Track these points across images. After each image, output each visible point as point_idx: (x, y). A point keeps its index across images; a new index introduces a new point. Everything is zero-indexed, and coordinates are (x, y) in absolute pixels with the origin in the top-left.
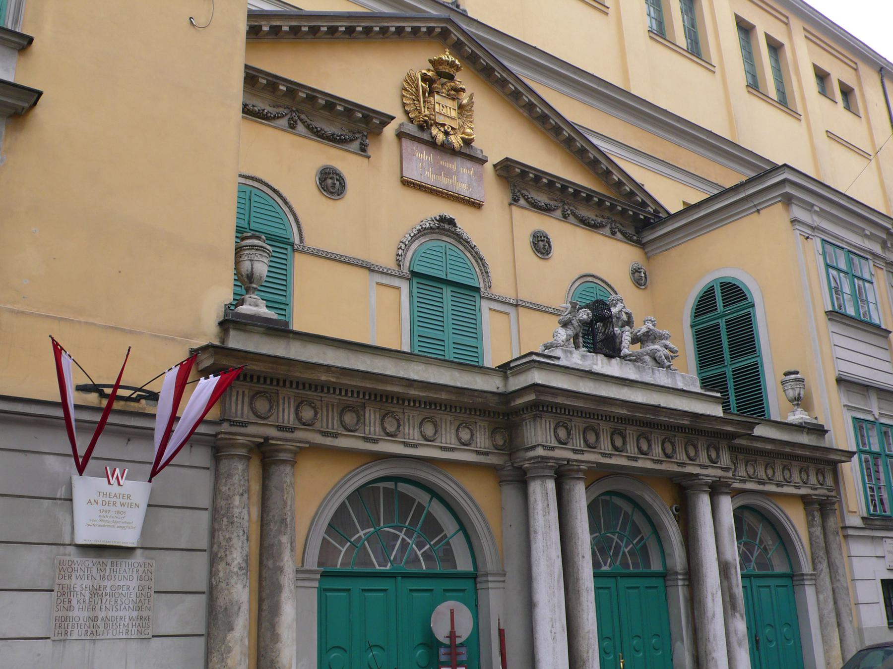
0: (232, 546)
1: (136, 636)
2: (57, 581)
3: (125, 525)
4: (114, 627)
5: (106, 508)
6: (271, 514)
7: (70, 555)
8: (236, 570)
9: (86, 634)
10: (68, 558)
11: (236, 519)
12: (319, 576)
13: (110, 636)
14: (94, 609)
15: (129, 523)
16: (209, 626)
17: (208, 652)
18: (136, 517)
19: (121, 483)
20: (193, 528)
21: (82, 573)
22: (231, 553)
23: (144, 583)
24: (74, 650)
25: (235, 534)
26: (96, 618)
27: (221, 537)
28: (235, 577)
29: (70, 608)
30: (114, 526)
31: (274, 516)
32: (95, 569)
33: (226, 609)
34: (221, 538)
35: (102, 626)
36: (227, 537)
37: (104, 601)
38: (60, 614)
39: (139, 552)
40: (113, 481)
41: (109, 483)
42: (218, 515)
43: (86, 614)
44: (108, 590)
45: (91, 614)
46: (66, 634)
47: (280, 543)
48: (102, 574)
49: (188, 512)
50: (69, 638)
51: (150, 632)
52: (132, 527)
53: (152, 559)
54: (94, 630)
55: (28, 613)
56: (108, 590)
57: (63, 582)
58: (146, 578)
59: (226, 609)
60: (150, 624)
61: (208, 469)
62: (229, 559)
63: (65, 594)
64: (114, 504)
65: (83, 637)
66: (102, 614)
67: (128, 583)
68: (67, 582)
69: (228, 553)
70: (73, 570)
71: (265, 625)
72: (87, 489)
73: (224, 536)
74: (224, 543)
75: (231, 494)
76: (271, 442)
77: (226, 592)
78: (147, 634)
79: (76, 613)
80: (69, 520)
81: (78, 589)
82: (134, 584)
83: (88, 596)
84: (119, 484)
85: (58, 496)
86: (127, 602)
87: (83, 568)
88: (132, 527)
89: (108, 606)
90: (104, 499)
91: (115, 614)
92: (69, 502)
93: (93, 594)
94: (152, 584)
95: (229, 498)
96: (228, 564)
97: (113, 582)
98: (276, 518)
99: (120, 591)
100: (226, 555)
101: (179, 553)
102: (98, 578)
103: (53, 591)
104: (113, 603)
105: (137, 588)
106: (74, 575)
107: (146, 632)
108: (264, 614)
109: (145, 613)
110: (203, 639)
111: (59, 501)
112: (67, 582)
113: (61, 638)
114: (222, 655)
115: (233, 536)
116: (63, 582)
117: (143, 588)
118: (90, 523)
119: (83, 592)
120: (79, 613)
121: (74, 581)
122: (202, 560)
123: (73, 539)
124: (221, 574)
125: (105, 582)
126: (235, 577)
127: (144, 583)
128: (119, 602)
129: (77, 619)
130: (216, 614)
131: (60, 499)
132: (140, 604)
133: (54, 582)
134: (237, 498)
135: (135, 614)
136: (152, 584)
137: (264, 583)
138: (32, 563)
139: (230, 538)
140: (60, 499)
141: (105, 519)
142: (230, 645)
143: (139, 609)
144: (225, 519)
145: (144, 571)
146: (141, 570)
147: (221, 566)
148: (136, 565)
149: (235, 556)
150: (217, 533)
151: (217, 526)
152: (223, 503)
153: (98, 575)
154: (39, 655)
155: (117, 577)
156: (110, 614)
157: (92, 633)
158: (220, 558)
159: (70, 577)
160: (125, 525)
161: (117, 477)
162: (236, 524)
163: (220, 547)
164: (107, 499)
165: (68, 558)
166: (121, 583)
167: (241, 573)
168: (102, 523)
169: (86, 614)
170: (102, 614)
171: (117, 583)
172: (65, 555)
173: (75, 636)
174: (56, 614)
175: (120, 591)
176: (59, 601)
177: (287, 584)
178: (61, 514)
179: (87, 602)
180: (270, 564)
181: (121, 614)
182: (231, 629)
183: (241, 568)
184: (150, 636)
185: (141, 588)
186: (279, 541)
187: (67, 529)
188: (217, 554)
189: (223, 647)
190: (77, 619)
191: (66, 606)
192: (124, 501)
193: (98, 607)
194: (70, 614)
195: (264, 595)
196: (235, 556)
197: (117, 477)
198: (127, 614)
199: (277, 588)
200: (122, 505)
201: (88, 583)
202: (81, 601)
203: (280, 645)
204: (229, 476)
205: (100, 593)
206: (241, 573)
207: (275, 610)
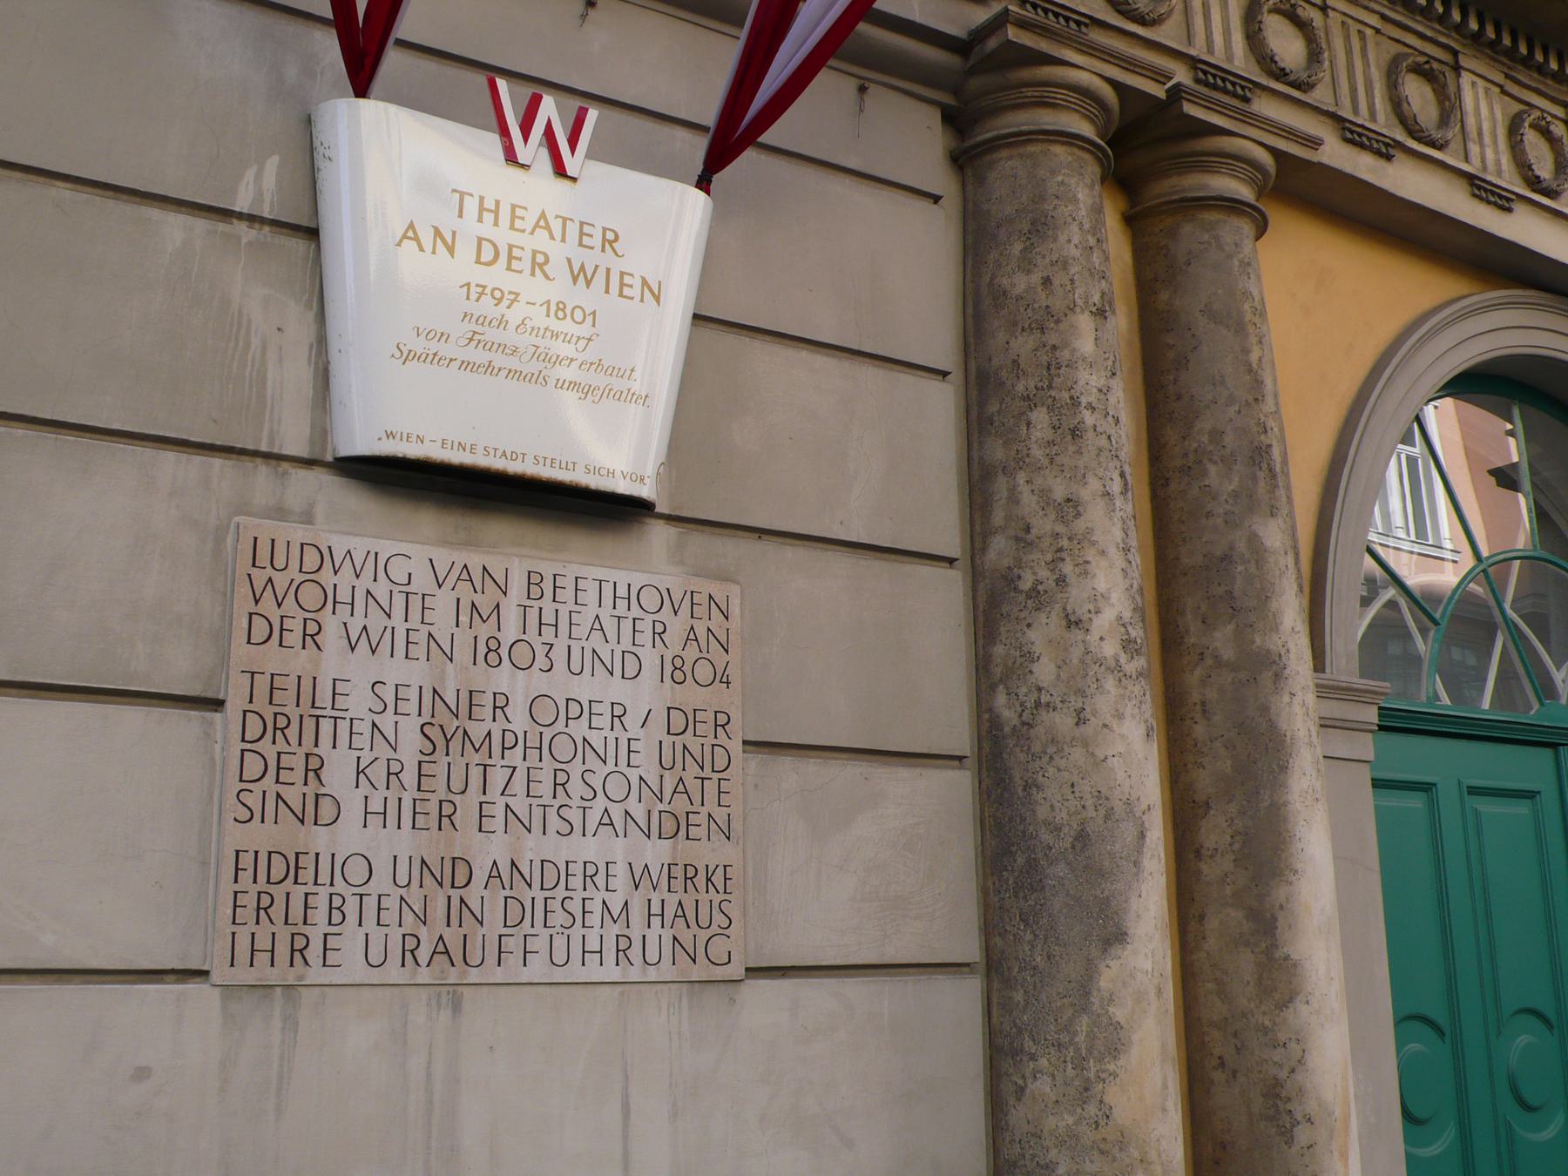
0: (1085, 539)
1: (666, 971)
2: (241, 652)
3: (600, 380)
4: (559, 918)
5: (497, 276)
6: (1204, 425)
7: (308, 518)
8: (1110, 649)
9: (409, 954)
10: (299, 534)
11: (1089, 418)
12: (1371, 715)
13: (538, 969)
14: (446, 818)
15: (612, 371)
16: (991, 925)
17: (1003, 1055)
18: (657, 345)
19: (572, 164)
20: (891, 454)
21: (376, 621)
22: (1084, 570)
23: (691, 696)
24: (354, 1039)
25: (1094, 484)
26: (456, 872)
27: (1026, 496)
28: (1110, 684)
29: (314, 811)
30: (539, 379)
31: (1216, 435)
32: (443, 604)
33: (1082, 837)
34: (1029, 501)
35: (494, 916)
36: (1059, 493)
37: (498, 777)
38: (260, 837)
39: (659, 535)
40: (532, 150)
41: (511, 157)
42: (994, 390)
43: (405, 843)
44: (519, 720)
45: (431, 845)
46: (298, 952)
47: (1258, 550)
48: (484, 631)
49: (870, 374)
50: (316, 974)
51: (740, 949)
52: (631, 397)
53: (726, 578)
54: (453, 938)
55: (82, 825)
56: (519, 720)
57: (272, 659)
58: (704, 672)
59: (1082, 837)
60: (733, 910)
61: (936, 199)
62: (1077, 597)
63: (287, 729)
64: (539, 265)
65: (394, 973)
66: (489, 850)
67: (617, 690)
68: (297, 661)
69: (1067, 568)
70: (330, 599)
71: (1223, 920)
72: (399, 162)
73: (1044, 495)
74: (1044, 525)
75: (1058, 304)
76: (1189, 109)
77: (1077, 754)
78: (713, 948)
79: (348, 836)
80: (300, 330)
81: (358, 702)
82: (645, 695)
83: (411, 746)
84: (560, 170)
85: (242, 204)
86: (616, 788)
87: (381, 590)
88: (631, 397)
89: (520, 805)
90: (486, 229)
91: (560, 850)
92: (299, 245)
93: (436, 740)
94: (730, 700)
95: (1046, 321)
96: (1073, 622)
97: (540, 682)
98: (1229, 439)
99: (579, 729)
100: (1061, 581)
101: (842, 563)
102: (463, 654)
103: (217, 704)
104: (545, 789)
105: (659, 717)
106: (332, 625)
107: (719, 948)
108: (1210, 870)
109: (707, 853)
110: (972, 988)
111: (241, 227)
112: (297, 661)
113: (273, 976)
114: (1080, 1064)
115: (1085, 494)
116: (272, 659)
117: (692, 721)
118: (419, 345)
119: (387, 722)
120: (364, 838)
121: (333, 661)
122: (941, 601)
123: (322, 430)
124: (1044, 672)
125: (503, 679)
126: (1110, 684)
127: (691, 696)
128: (576, 787)
129: (357, 871)
130: (1032, 865)
131: (252, 219)
132: (681, 804)
133: (224, 658)
134: (1085, 322)
135: (656, 853)
136: (730, 700)
137: (1200, 731)
138: (105, 545)
139: (1072, 506)
140: (252, 219)
141: (492, 335)
142: (1119, 1013)
143: (680, 827)
144: (1040, 417)
145: (691, 637)
146: (677, 627)
147: (1042, 632)
148: (650, 600)
149: (1101, 584)
150: (1001, 485)
151: (996, 451)
152: (1023, 345)
153: (464, 638)
154: (142, 1074)
155: (559, 654)
156: (533, 848)
157: (441, 949)
158: (1034, 593)
159: (312, 638)
160: (600, 380)
161: (549, 133)
162: (1091, 441)
163: (1024, 538)
164: (503, 236)
165: (299, 534)
166: (583, 689)
167: (1131, 667)
168: (480, 356)
169: (405, 843)
170: (489, 850)
171: (561, 685)
172: (280, 513)
173: (352, 967)
174: (237, 837)
175: (579, 729)
176: (253, 767)
177: (1302, 734)
178: (250, 285)
179: (409, 777)
180: (1222, 640)
181: (589, 849)
182: (1116, 937)
183: (1127, 644)
184: (735, 970)
185: (681, 721)
186: (1254, 539)
187: (294, 375)
188: (1010, 580)
189: (1083, 1025)
190: (357, 871)
191: (293, 795)
192: (591, 259)
193: (467, 807)
194: (319, 839)
195: (1204, 781)
196: (1101, 584)
197: (549, 133)
198: (617, 850)
199: (1262, 754)
200: (581, 275)
201: (415, 674)
202: (378, 773)
203: (1301, 1013)
204: (1040, 227)
205: (477, 731)
206: (1131, 667)
207: (1267, 853)
